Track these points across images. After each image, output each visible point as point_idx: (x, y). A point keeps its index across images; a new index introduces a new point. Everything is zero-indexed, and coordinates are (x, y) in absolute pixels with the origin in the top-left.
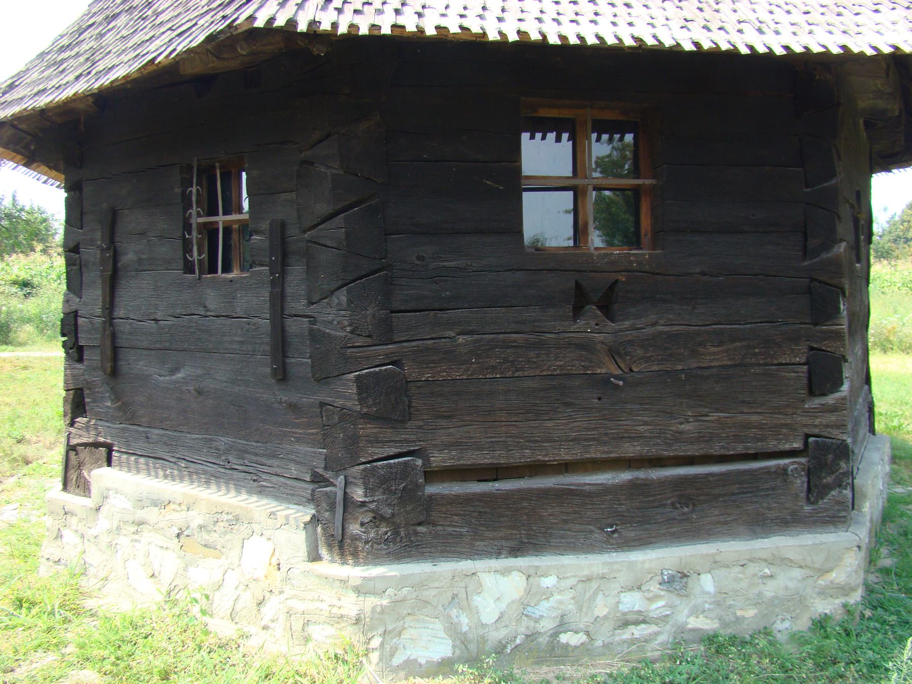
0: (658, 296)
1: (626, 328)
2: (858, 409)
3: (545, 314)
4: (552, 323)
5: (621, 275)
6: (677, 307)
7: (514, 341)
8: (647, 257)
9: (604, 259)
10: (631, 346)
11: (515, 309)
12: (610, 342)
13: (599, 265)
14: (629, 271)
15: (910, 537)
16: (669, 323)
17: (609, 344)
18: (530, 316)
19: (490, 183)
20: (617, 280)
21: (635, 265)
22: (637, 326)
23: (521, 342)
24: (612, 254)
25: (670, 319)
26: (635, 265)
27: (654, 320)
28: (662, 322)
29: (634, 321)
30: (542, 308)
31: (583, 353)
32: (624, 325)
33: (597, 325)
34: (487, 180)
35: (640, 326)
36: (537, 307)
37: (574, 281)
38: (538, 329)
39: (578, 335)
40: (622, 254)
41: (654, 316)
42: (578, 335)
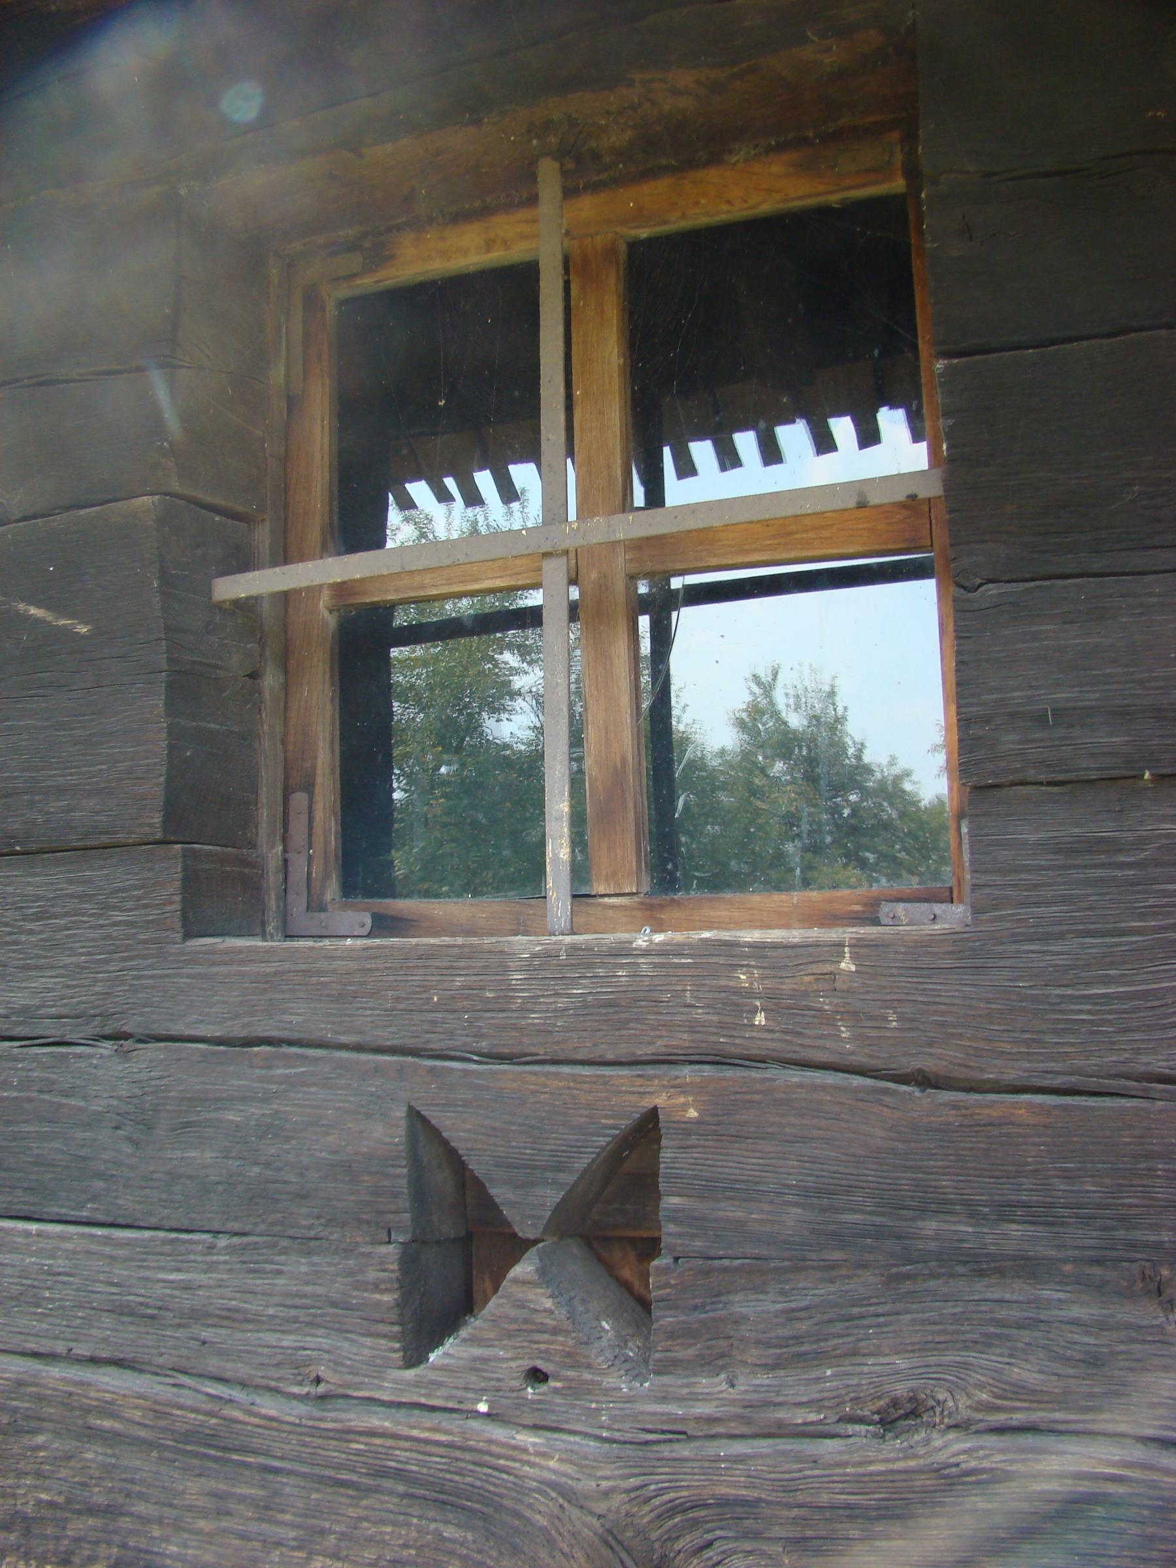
0: (930, 1226)
1: (712, 1420)
2: (691, 844)
3: (258, 1282)
4: (288, 1341)
5: (683, 1089)
6: (1076, 1312)
7: (107, 1409)
8: (847, 965)
9: (574, 982)
10: (746, 1536)
11: (120, 1244)
12: (607, 1494)
13: (535, 1018)
14: (721, 1060)
15: (1169, 1292)
16: (1019, 1418)
17: (601, 1507)
18: (187, 1287)
19: (33, 611)
20: (653, 1113)
21: (760, 1019)
22: (781, 1414)
23: (138, 1415)
24: (623, 951)
25: (1020, 1391)
26: (760, 1019)
27: (901, 1389)
28: (961, 1405)
29: (763, 1379)
30: (244, 1248)
31: (449, 1532)
32: (694, 1398)
33: (537, 1376)
34: (30, 603)
35: (800, 1417)
36: (223, 1241)
37: (400, 1112)
38: (213, 1364)
39: (421, 1427)
40: (676, 950)
41: (901, 1363)
42: (421, 1427)
